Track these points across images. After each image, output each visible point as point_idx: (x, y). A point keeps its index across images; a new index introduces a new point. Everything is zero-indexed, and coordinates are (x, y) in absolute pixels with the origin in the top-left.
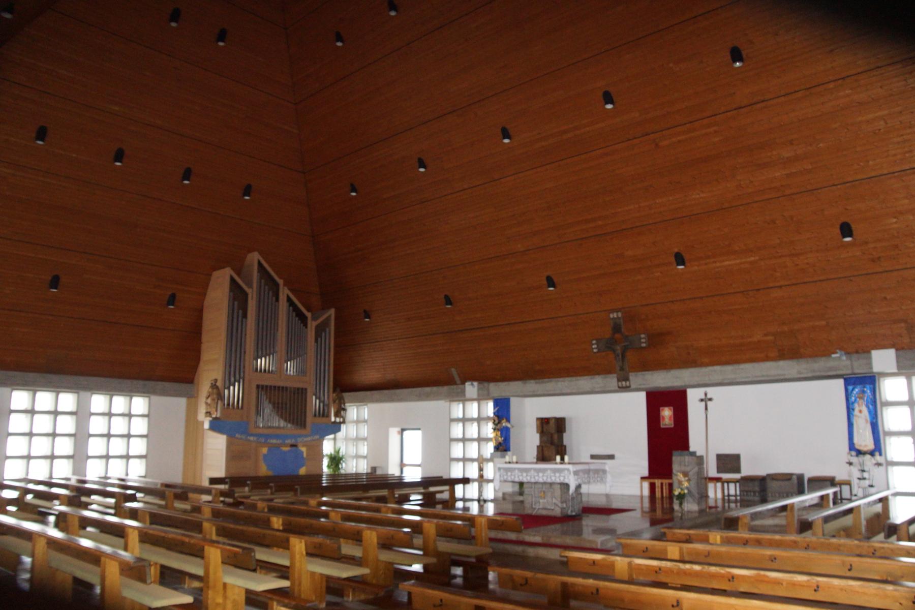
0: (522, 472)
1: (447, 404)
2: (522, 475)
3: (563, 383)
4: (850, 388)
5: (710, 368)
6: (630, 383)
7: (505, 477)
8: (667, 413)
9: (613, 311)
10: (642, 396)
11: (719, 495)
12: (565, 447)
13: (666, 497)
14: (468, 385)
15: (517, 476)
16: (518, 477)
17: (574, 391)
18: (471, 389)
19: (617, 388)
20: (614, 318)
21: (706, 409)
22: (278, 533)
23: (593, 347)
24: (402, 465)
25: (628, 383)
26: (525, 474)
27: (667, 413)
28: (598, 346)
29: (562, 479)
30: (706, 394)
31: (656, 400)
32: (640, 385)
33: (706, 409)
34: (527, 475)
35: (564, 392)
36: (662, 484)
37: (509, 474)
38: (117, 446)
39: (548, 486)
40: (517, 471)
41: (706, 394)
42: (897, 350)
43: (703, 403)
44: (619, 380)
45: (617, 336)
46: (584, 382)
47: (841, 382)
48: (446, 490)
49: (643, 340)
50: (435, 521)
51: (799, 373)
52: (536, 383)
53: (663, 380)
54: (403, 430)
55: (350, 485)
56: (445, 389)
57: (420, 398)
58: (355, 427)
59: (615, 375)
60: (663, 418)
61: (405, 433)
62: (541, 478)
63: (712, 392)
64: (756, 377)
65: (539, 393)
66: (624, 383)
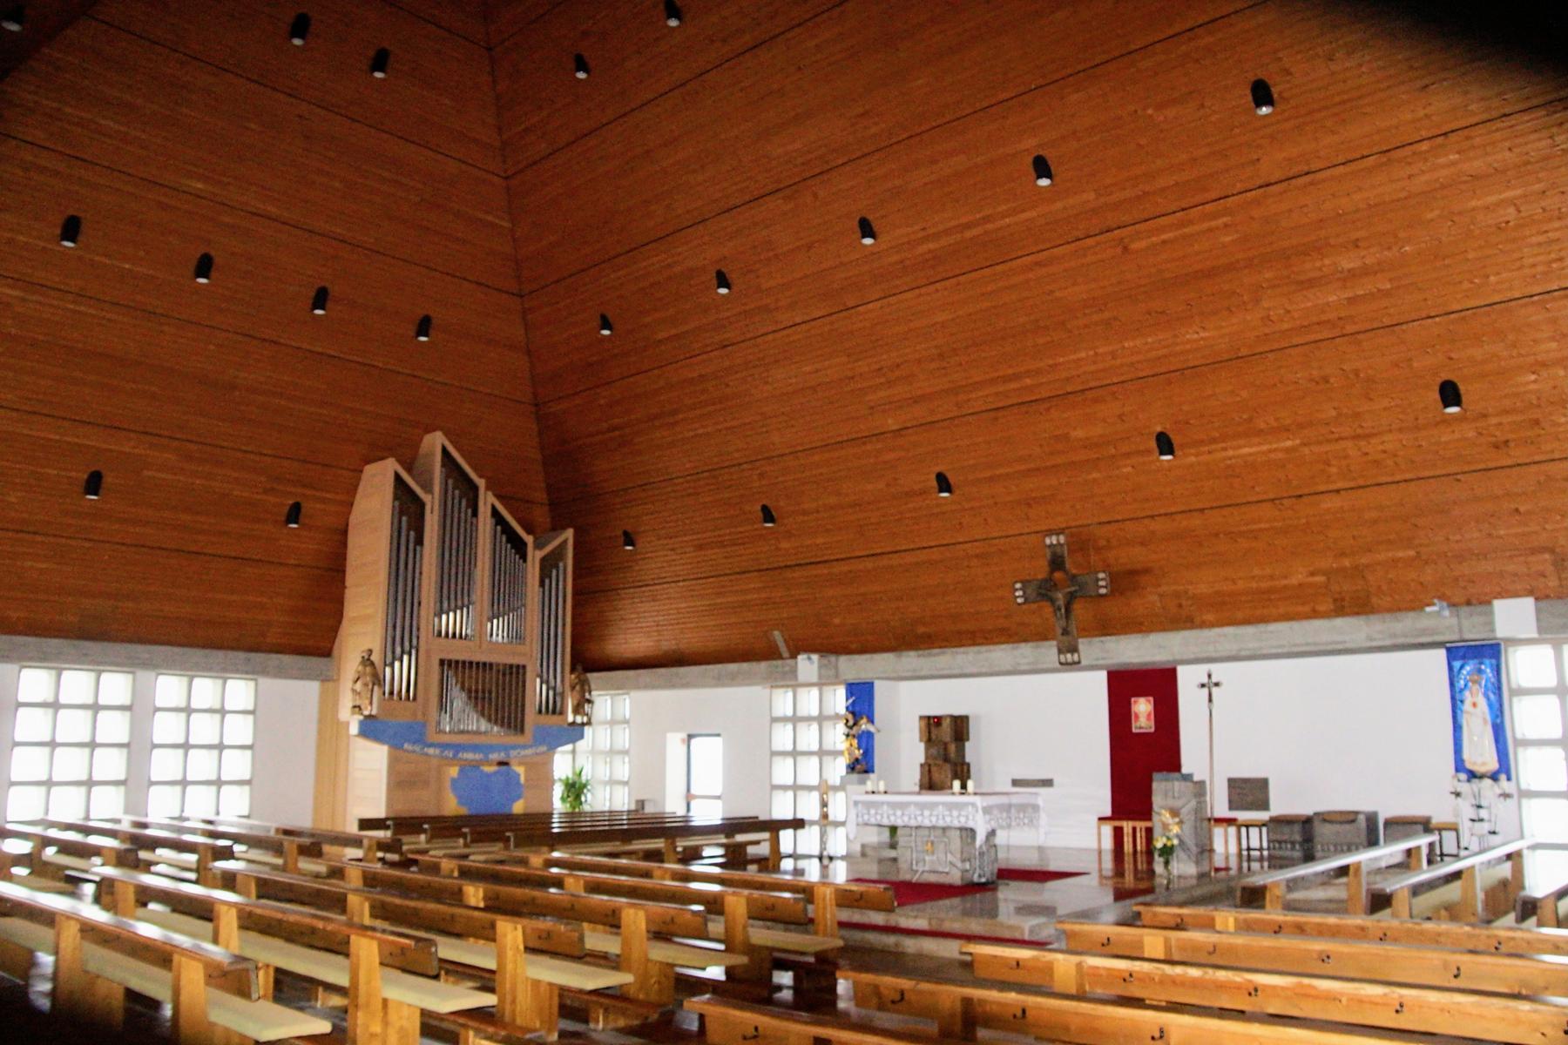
1: (768, 691)
2: (894, 814)
3: (964, 656)
4: (1457, 664)
7: (866, 817)
8: (1143, 708)
10: (1101, 678)
11: (1233, 849)
12: (968, 765)
15: (885, 816)
16: (888, 817)
17: (984, 670)
18: (807, 665)
19: (1058, 665)
20: (1051, 546)
23: (1017, 594)
24: (689, 797)
25: (1076, 657)
27: (1143, 708)
28: (1024, 593)
29: (963, 820)
31: (1124, 685)
32: (1097, 659)
34: (903, 814)
35: (967, 671)
36: (1134, 829)
37: (927, 813)
40: (885, 807)
44: (1060, 651)
45: (1058, 575)
46: (1001, 654)
47: (1441, 654)
49: (1102, 583)
50: (746, 892)
54: (690, 737)
56: (763, 666)
57: (719, 682)
60: (1137, 717)
61: (694, 742)
63: (1220, 671)
65: (923, 673)
66: (1069, 656)
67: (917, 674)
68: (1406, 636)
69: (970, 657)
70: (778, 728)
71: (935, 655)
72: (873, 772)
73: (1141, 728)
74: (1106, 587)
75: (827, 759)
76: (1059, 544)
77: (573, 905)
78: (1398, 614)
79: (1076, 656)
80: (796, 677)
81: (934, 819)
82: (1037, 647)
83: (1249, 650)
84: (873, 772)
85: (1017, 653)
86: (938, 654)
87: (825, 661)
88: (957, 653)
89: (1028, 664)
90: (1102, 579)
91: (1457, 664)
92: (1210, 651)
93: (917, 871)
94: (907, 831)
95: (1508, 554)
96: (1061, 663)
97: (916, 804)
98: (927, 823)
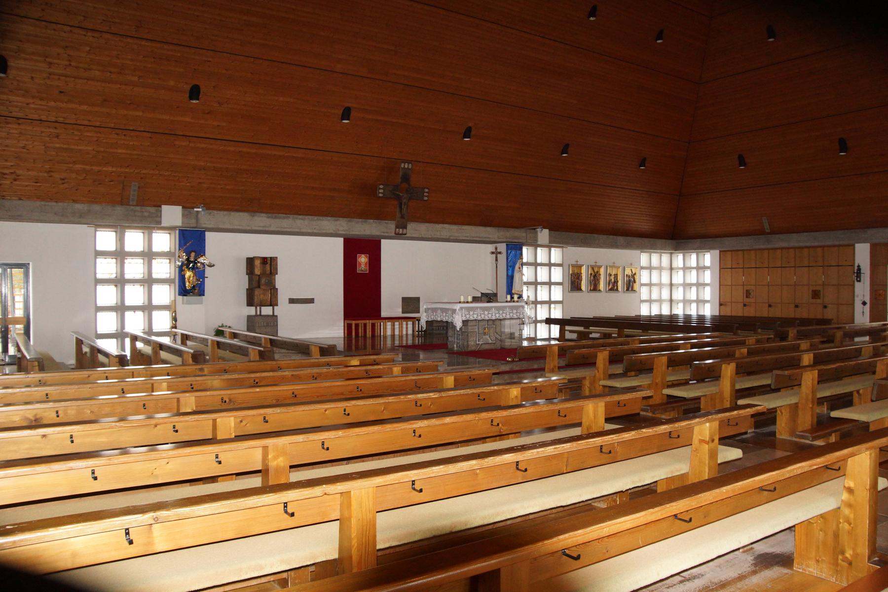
0: (512, 310)
2: (484, 314)
3: (302, 221)
5: (441, 225)
6: (396, 230)
8: (363, 260)
9: (405, 162)
10: (342, 239)
11: (410, 332)
12: (277, 289)
13: (362, 336)
14: (165, 209)
15: (494, 314)
17: (315, 231)
19: (394, 235)
21: (497, 260)
22: (452, 393)
23: (427, 194)
25: (405, 231)
26: (486, 313)
27: (363, 260)
29: (475, 316)
30: (496, 248)
31: (352, 248)
32: (384, 233)
33: (497, 260)
34: (489, 313)
36: (357, 326)
37: (471, 313)
38: (542, 274)
39: (490, 323)
41: (496, 248)
42: (183, 207)
43: (494, 255)
44: (397, 227)
48: (123, 349)
49: (381, 191)
50: (608, 349)
51: (499, 238)
52: (268, 217)
53: (364, 229)
55: (348, 335)
58: (652, 265)
59: (394, 222)
60: (360, 264)
62: (487, 316)
64: (473, 237)
65: (271, 229)
66: (401, 230)
67: (267, 229)
68: (509, 239)
69: (306, 222)
70: (559, 261)
71: (280, 218)
72: (204, 295)
73: (362, 271)
74: (379, 193)
75: (533, 280)
76: (408, 168)
77: (728, 353)
78: (508, 229)
79: (405, 230)
80: (160, 223)
81: (490, 316)
82: (349, 221)
83: (455, 236)
84: (204, 295)
85: (338, 223)
86: (284, 218)
87: (186, 212)
88: (297, 218)
89: (343, 230)
90: (381, 189)
91: (509, 251)
92: (438, 235)
93: (479, 344)
94: (474, 323)
95: (66, 180)
96: (395, 234)
97: (481, 308)
98: (487, 318)
